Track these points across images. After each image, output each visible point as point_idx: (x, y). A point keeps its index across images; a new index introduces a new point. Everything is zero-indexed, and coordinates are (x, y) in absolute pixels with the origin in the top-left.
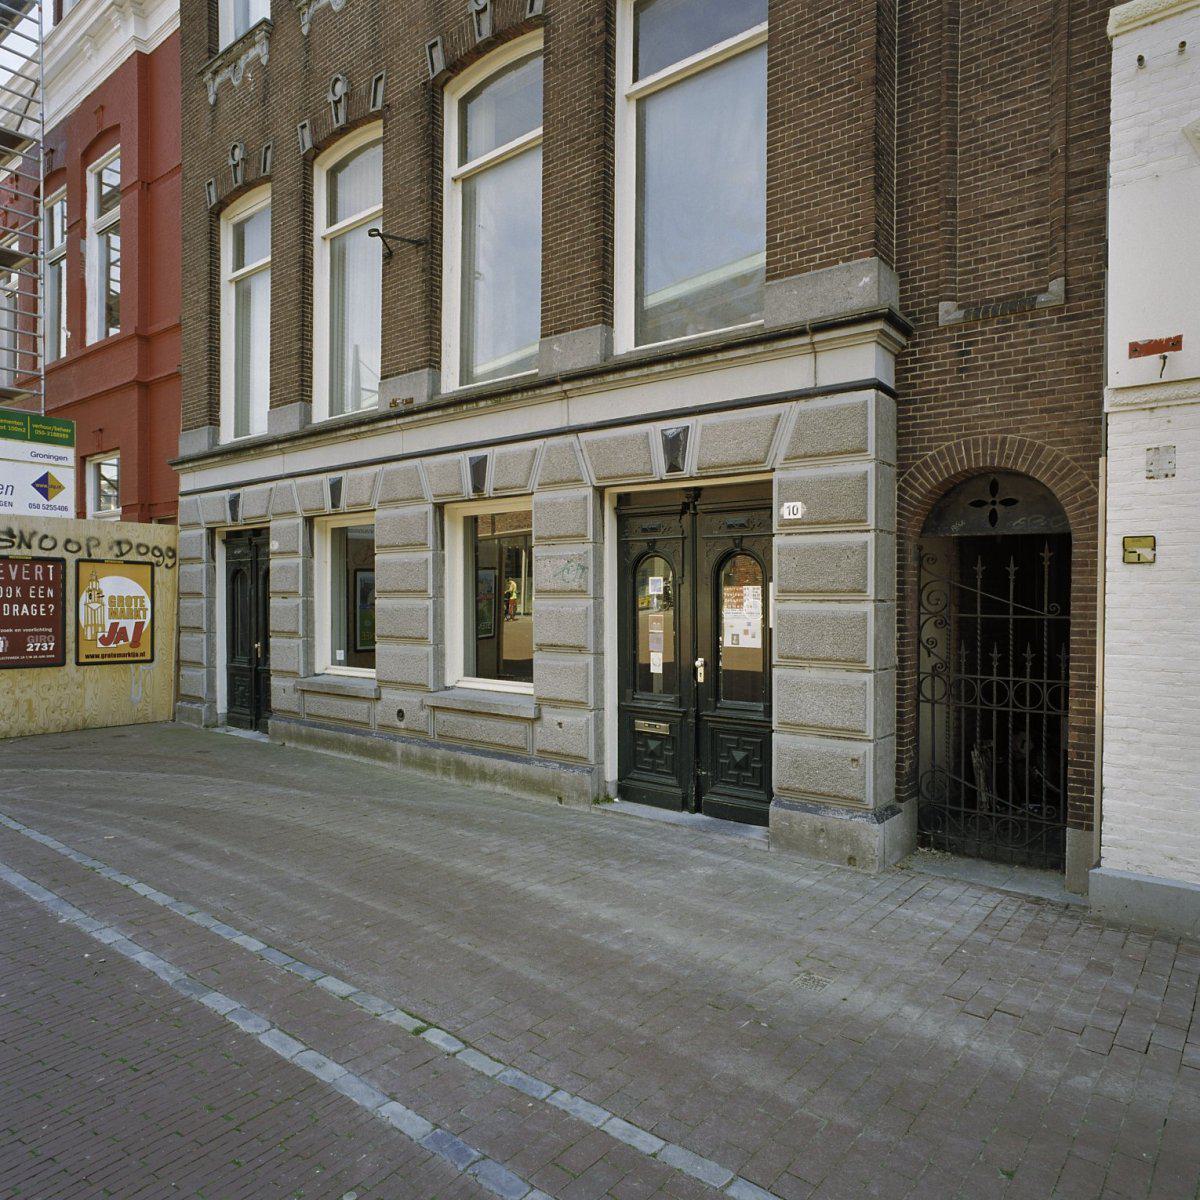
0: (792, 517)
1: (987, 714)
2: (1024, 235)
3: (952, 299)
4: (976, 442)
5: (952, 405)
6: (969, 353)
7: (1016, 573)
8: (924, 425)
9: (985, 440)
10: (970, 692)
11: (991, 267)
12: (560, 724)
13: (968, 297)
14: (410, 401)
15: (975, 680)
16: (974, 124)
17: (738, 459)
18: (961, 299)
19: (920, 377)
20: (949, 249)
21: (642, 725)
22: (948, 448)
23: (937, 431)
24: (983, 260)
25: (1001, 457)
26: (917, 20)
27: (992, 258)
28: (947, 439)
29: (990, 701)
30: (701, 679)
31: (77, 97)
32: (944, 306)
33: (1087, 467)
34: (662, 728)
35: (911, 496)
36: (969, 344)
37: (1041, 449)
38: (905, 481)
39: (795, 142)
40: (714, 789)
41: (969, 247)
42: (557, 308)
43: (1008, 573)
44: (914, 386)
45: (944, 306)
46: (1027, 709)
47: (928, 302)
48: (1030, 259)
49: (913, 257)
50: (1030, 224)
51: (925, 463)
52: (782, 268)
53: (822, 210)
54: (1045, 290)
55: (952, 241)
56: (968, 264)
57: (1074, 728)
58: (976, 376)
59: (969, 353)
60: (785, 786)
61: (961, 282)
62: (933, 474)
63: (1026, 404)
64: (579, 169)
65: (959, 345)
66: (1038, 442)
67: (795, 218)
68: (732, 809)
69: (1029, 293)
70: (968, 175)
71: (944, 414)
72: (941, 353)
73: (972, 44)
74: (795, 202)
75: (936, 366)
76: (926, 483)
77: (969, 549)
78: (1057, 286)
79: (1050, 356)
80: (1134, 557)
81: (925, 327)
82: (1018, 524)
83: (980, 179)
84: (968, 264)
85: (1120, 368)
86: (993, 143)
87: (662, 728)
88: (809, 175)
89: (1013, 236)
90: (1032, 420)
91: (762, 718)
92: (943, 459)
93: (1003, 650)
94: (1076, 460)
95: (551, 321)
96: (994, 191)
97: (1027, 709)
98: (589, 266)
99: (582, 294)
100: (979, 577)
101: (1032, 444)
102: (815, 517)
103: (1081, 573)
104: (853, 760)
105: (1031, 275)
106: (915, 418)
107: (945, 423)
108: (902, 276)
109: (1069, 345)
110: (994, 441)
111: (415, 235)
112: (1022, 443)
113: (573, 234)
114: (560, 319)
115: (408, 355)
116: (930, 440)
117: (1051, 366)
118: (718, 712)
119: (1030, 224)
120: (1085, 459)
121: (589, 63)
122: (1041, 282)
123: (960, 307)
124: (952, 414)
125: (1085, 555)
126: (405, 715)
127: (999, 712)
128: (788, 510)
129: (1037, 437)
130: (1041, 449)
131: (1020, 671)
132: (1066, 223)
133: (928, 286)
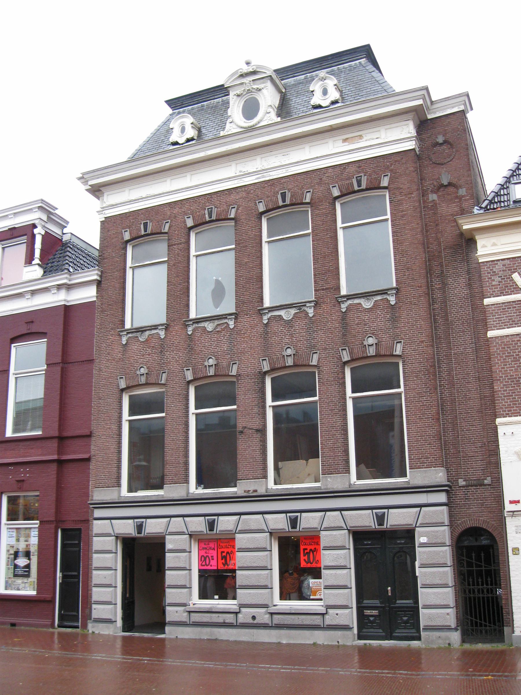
0: (423, 542)
1: (470, 598)
2: (479, 463)
3: (461, 478)
4: (472, 519)
5: (464, 509)
6: (467, 494)
7: (484, 556)
8: (457, 514)
9: (474, 519)
10: (465, 591)
11: (471, 471)
12: (337, 614)
13: (466, 478)
14: (255, 491)
15: (475, 588)
16: (463, 431)
17: (404, 523)
18: (464, 478)
19: (455, 499)
20: (460, 464)
21: (368, 612)
22: (464, 521)
23: (461, 516)
24: (469, 468)
25: (479, 524)
26: (445, 399)
27: (472, 468)
28: (464, 518)
29: (480, 594)
30: (390, 594)
31: (11, 312)
32: (460, 480)
33: (501, 528)
34: (375, 612)
35: (455, 534)
36: (467, 492)
37: (489, 522)
38: (453, 530)
39: (416, 430)
40: (396, 631)
41: (465, 464)
42: (328, 465)
43: (481, 556)
44: (453, 502)
45: (460, 480)
46: (472, 595)
47: (455, 478)
48: (481, 470)
49: (450, 465)
50: (480, 461)
51: (458, 525)
52: (414, 466)
53: (425, 451)
54: (486, 479)
55: (460, 462)
56: (465, 469)
57: (504, 599)
58: (470, 501)
59: (467, 494)
60: (426, 625)
61: (464, 473)
62: (460, 528)
63: (484, 510)
64: (335, 420)
65: (465, 492)
66: (488, 520)
67: (418, 452)
68: (402, 636)
69: (482, 479)
70: (463, 444)
71: (462, 511)
72: (460, 494)
73: (460, 409)
74: (417, 448)
75: (459, 497)
76: (460, 530)
77: (470, 549)
78: (489, 479)
79: (489, 497)
80: (514, 553)
81: (455, 485)
82: (485, 542)
83: (466, 446)
84: (465, 469)
85: (508, 507)
86: (469, 437)
87: (375, 612)
88: (421, 441)
89: (477, 463)
90: (486, 514)
91: (413, 605)
92: (463, 524)
93: (482, 578)
94: (498, 525)
95: (325, 470)
96: (471, 450)
97: (472, 595)
98: (341, 453)
99: (339, 462)
100: (474, 557)
101: (486, 521)
102: (430, 542)
103: (502, 556)
104: (448, 614)
105: (482, 474)
106: (454, 511)
107: (463, 513)
108: (447, 470)
109: (493, 495)
110: (476, 519)
111: (255, 427)
112: (484, 520)
113: (334, 441)
114: (329, 470)
115: (253, 472)
116: (459, 518)
117: (489, 500)
118: (397, 605)
119: (480, 461)
120: (500, 525)
121: (338, 387)
122: (485, 477)
123: (464, 481)
124: (465, 511)
125: (502, 551)
126: (257, 618)
127: (491, 597)
128: (421, 539)
129: (488, 519)
130: (489, 522)
131: (487, 584)
132: (490, 463)
133: (455, 474)
